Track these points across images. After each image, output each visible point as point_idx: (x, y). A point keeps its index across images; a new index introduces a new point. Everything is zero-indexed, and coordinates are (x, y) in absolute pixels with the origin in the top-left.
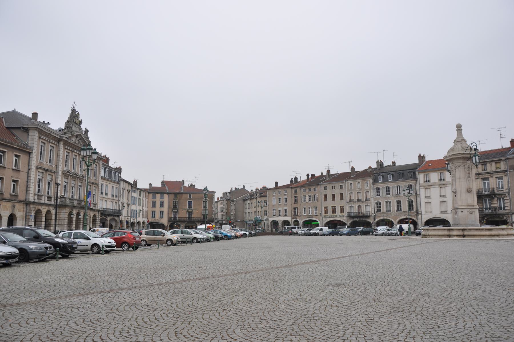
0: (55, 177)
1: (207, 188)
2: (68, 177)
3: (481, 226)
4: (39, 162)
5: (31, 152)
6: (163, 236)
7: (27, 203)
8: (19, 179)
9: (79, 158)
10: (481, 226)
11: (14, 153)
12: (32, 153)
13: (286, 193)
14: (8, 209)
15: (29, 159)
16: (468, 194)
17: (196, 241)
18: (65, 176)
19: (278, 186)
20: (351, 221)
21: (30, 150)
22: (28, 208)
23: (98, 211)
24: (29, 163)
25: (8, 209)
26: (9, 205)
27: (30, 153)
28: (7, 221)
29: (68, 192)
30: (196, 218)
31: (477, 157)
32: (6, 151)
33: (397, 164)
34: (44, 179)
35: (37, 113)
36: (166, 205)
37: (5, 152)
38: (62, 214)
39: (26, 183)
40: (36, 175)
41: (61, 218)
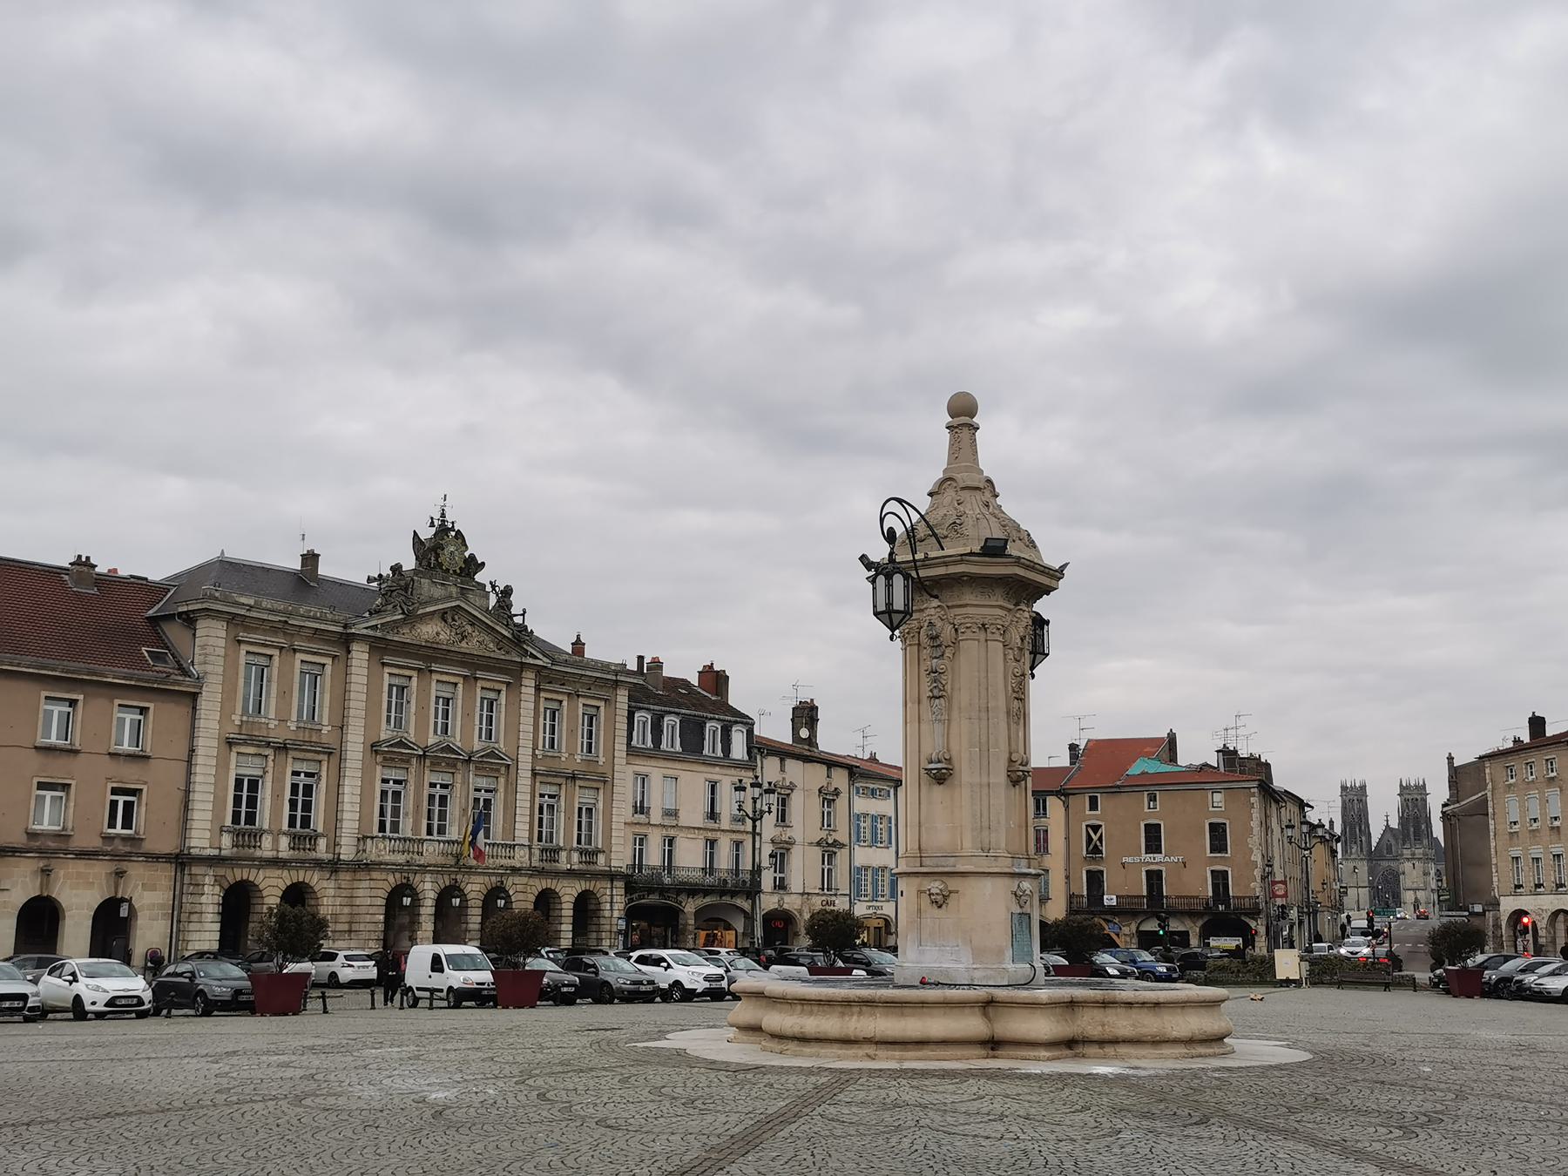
0: (334, 771)
1: (1453, 755)
2: (408, 761)
3: (193, 976)
4: (237, 723)
5: (197, 690)
6: (666, 969)
7: (182, 861)
8: (145, 783)
9: (469, 693)
10: (973, 963)
11: (117, 702)
12: (201, 693)
13: (1554, 774)
14: (93, 883)
15: (194, 718)
16: (938, 790)
17: (679, 994)
18: (385, 759)
19: (1547, 735)
20: (1200, 923)
21: (194, 687)
22: (187, 879)
23: (611, 876)
24: (193, 727)
25: (93, 883)
26: (99, 871)
27: (194, 697)
28: (88, 924)
29: (410, 816)
30: (1177, 897)
31: (898, 580)
32: (81, 697)
33: (590, 653)
34: (269, 777)
35: (93, 561)
36: (1056, 842)
37: (76, 701)
38: (360, 893)
39: (181, 794)
40: (222, 765)
41: (356, 910)
